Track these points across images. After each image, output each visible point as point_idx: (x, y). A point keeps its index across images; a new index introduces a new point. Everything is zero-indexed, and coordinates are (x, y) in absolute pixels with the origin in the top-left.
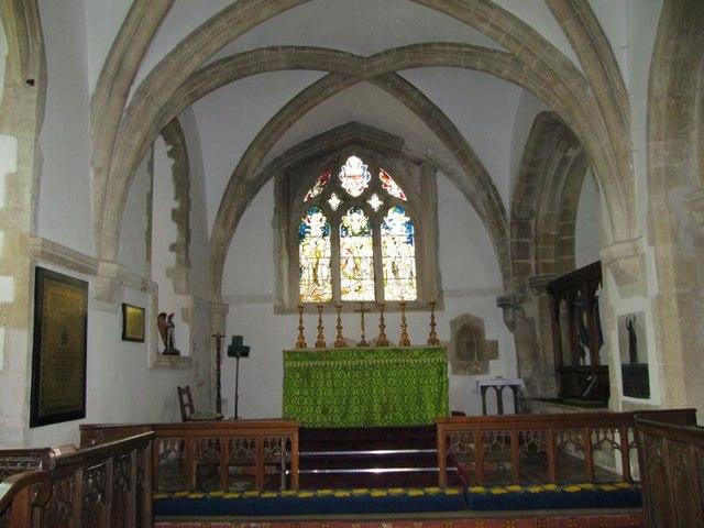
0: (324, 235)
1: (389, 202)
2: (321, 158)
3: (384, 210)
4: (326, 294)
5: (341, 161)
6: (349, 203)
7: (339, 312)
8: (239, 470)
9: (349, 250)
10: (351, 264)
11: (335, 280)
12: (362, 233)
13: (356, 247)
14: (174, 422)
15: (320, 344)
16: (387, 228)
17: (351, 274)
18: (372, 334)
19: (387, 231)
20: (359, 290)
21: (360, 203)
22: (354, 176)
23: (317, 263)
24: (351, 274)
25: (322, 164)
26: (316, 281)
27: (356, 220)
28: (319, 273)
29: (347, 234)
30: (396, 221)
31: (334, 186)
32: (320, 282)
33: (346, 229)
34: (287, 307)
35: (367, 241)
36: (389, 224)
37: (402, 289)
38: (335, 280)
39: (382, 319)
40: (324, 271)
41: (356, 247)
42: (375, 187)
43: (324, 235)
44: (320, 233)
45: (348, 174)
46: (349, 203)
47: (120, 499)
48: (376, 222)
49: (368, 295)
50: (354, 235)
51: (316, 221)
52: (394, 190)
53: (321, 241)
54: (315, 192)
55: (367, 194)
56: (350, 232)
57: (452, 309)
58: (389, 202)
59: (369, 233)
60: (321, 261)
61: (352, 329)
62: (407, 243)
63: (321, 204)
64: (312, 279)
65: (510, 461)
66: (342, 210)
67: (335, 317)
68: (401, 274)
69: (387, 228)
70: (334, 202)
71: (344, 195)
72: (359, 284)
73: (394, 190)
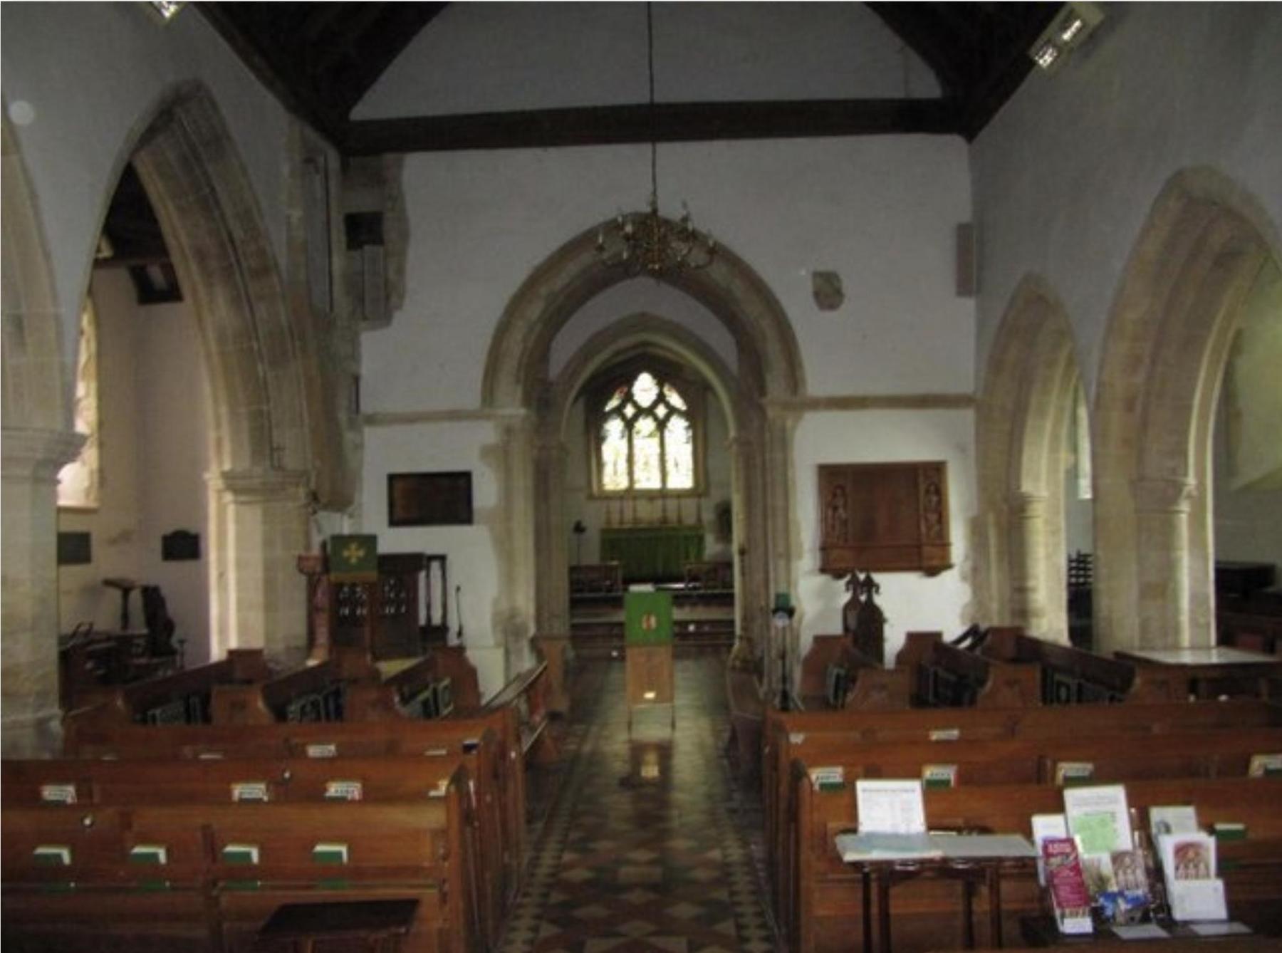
2: (621, 378)
3: (668, 417)
4: (623, 484)
6: (641, 412)
11: (631, 473)
12: (651, 435)
13: (646, 446)
14: (902, 829)
15: (621, 522)
18: (657, 515)
20: (648, 480)
21: (649, 412)
22: (645, 388)
30: (678, 429)
31: (629, 398)
34: (394, 689)
35: (656, 441)
37: (682, 478)
38: (631, 473)
40: (623, 466)
41: (646, 446)
42: (661, 398)
46: (641, 412)
48: (661, 425)
49: (655, 484)
51: (614, 427)
52: (675, 400)
54: (613, 403)
57: (716, 496)
58: (672, 411)
61: (648, 512)
63: (619, 411)
65: (362, 605)
66: (636, 417)
67: (631, 503)
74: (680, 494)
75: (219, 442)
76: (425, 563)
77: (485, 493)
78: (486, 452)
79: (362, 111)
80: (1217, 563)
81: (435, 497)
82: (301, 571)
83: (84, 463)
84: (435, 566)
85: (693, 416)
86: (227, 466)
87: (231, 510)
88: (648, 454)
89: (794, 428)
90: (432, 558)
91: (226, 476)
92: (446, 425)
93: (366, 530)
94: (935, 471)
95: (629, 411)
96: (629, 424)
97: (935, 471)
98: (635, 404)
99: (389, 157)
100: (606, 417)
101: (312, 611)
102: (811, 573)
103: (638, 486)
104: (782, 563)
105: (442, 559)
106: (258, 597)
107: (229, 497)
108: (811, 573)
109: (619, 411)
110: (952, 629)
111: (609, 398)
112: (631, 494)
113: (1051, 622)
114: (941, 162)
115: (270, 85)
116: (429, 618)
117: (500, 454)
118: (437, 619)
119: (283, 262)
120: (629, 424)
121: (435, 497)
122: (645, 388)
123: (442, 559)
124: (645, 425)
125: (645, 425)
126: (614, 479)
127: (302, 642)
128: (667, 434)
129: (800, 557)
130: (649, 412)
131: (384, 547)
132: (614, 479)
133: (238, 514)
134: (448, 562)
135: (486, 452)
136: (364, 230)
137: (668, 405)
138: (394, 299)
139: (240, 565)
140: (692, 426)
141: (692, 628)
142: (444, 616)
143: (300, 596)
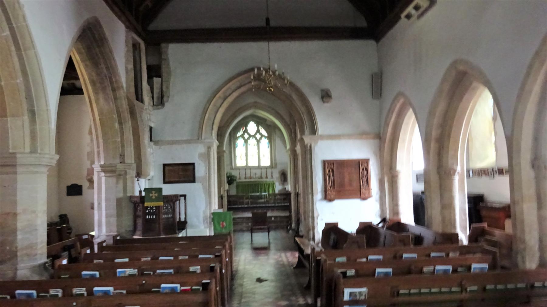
2: (244, 123)
4: (244, 164)
11: (247, 160)
20: (253, 162)
22: (252, 127)
30: (265, 142)
31: (246, 131)
37: (266, 162)
38: (247, 160)
42: (258, 131)
48: (258, 141)
51: (240, 142)
52: (263, 132)
57: (280, 168)
58: (262, 136)
74: (266, 168)
75: (99, 153)
76: (179, 198)
77: (200, 171)
78: (201, 155)
79: (152, 27)
80: (468, 192)
81: (183, 173)
82: (131, 202)
83: (139, 230)
84: (182, 199)
85: (269, 138)
86: (102, 163)
87: (103, 179)
88: (254, 152)
89: (314, 146)
90: (181, 196)
91: (101, 166)
92: (185, 146)
93: (156, 186)
94: (367, 161)
95: (246, 136)
96: (246, 141)
97: (367, 161)
98: (249, 134)
99: (163, 45)
100: (237, 138)
101: (136, 217)
102: (321, 200)
103: (249, 165)
104: (310, 196)
105: (185, 196)
106: (114, 212)
107: (103, 174)
108: (321, 200)
109: (242, 136)
110: (375, 220)
111: (239, 130)
112: (247, 168)
113: (407, 216)
114: (366, 46)
115: (120, 18)
116: (180, 218)
117: (207, 157)
118: (183, 219)
119: (125, 85)
120: (246, 141)
121: (183, 173)
122: (252, 127)
123: (185, 196)
124: (252, 141)
125: (252, 141)
126: (240, 162)
127: (131, 228)
128: (260, 144)
129: (317, 193)
130: (254, 136)
131: (164, 193)
132: (240, 162)
133: (106, 180)
134: (187, 197)
135: (201, 155)
136: (155, 71)
137: (261, 134)
138: (165, 99)
139: (107, 200)
140: (270, 142)
141: (273, 219)
142: (185, 218)
143: (131, 211)
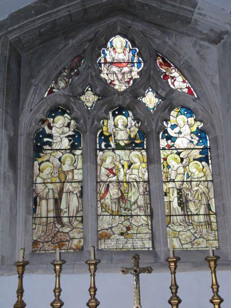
0: (73, 147)
1: (169, 101)
5: (100, 43)
7: (58, 274)
8: (98, 145)
9: (111, 170)
10: (114, 191)
12: (132, 145)
16: (169, 138)
17: (114, 208)
19: (177, 130)
21: (126, 103)
23: (61, 192)
24: (114, 208)
25: (71, 42)
26: (58, 218)
27: (121, 126)
28: (63, 206)
29: (108, 145)
32: (65, 220)
33: (107, 139)
36: (171, 133)
39: (174, 287)
42: (151, 78)
43: (73, 147)
44: (66, 144)
45: (109, 60)
47: (216, 109)
48: (149, 137)
50: (118, 147)
52: (179, 83)
53: (68, 158)
55: (136, 91)
56: (113, 144)
58: (169, 101)
59: (141, 145)
60: (68, 186)
62: (200, 160)
64: (51, 214)
68: (192, 208)
69: (169, 138)
70: (89, 99)
71: (105, 91)
72: (127, 223)
73: (179, 83)
